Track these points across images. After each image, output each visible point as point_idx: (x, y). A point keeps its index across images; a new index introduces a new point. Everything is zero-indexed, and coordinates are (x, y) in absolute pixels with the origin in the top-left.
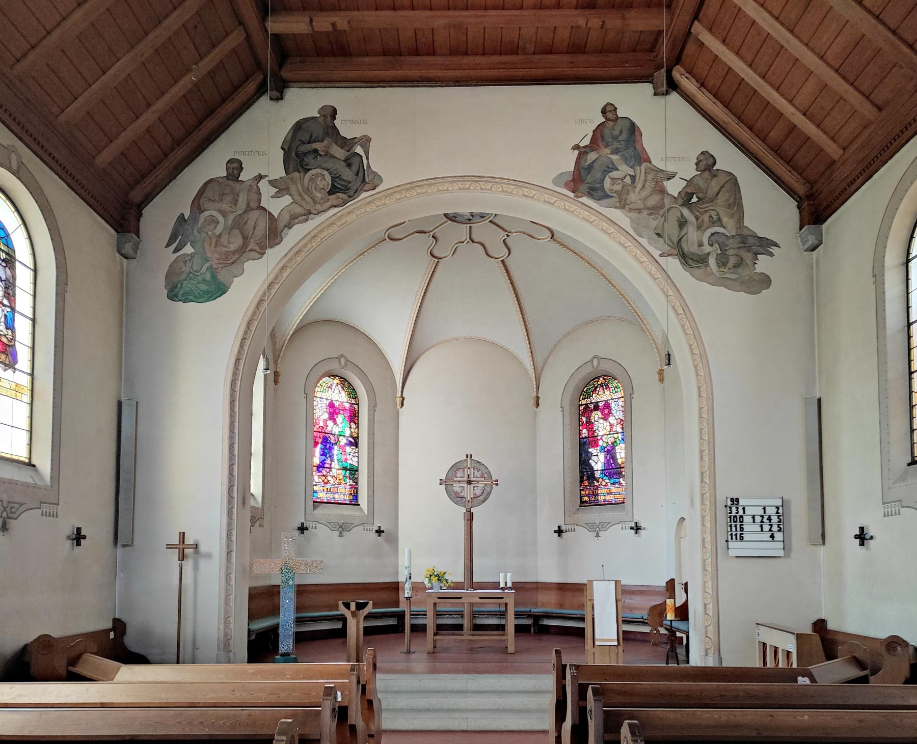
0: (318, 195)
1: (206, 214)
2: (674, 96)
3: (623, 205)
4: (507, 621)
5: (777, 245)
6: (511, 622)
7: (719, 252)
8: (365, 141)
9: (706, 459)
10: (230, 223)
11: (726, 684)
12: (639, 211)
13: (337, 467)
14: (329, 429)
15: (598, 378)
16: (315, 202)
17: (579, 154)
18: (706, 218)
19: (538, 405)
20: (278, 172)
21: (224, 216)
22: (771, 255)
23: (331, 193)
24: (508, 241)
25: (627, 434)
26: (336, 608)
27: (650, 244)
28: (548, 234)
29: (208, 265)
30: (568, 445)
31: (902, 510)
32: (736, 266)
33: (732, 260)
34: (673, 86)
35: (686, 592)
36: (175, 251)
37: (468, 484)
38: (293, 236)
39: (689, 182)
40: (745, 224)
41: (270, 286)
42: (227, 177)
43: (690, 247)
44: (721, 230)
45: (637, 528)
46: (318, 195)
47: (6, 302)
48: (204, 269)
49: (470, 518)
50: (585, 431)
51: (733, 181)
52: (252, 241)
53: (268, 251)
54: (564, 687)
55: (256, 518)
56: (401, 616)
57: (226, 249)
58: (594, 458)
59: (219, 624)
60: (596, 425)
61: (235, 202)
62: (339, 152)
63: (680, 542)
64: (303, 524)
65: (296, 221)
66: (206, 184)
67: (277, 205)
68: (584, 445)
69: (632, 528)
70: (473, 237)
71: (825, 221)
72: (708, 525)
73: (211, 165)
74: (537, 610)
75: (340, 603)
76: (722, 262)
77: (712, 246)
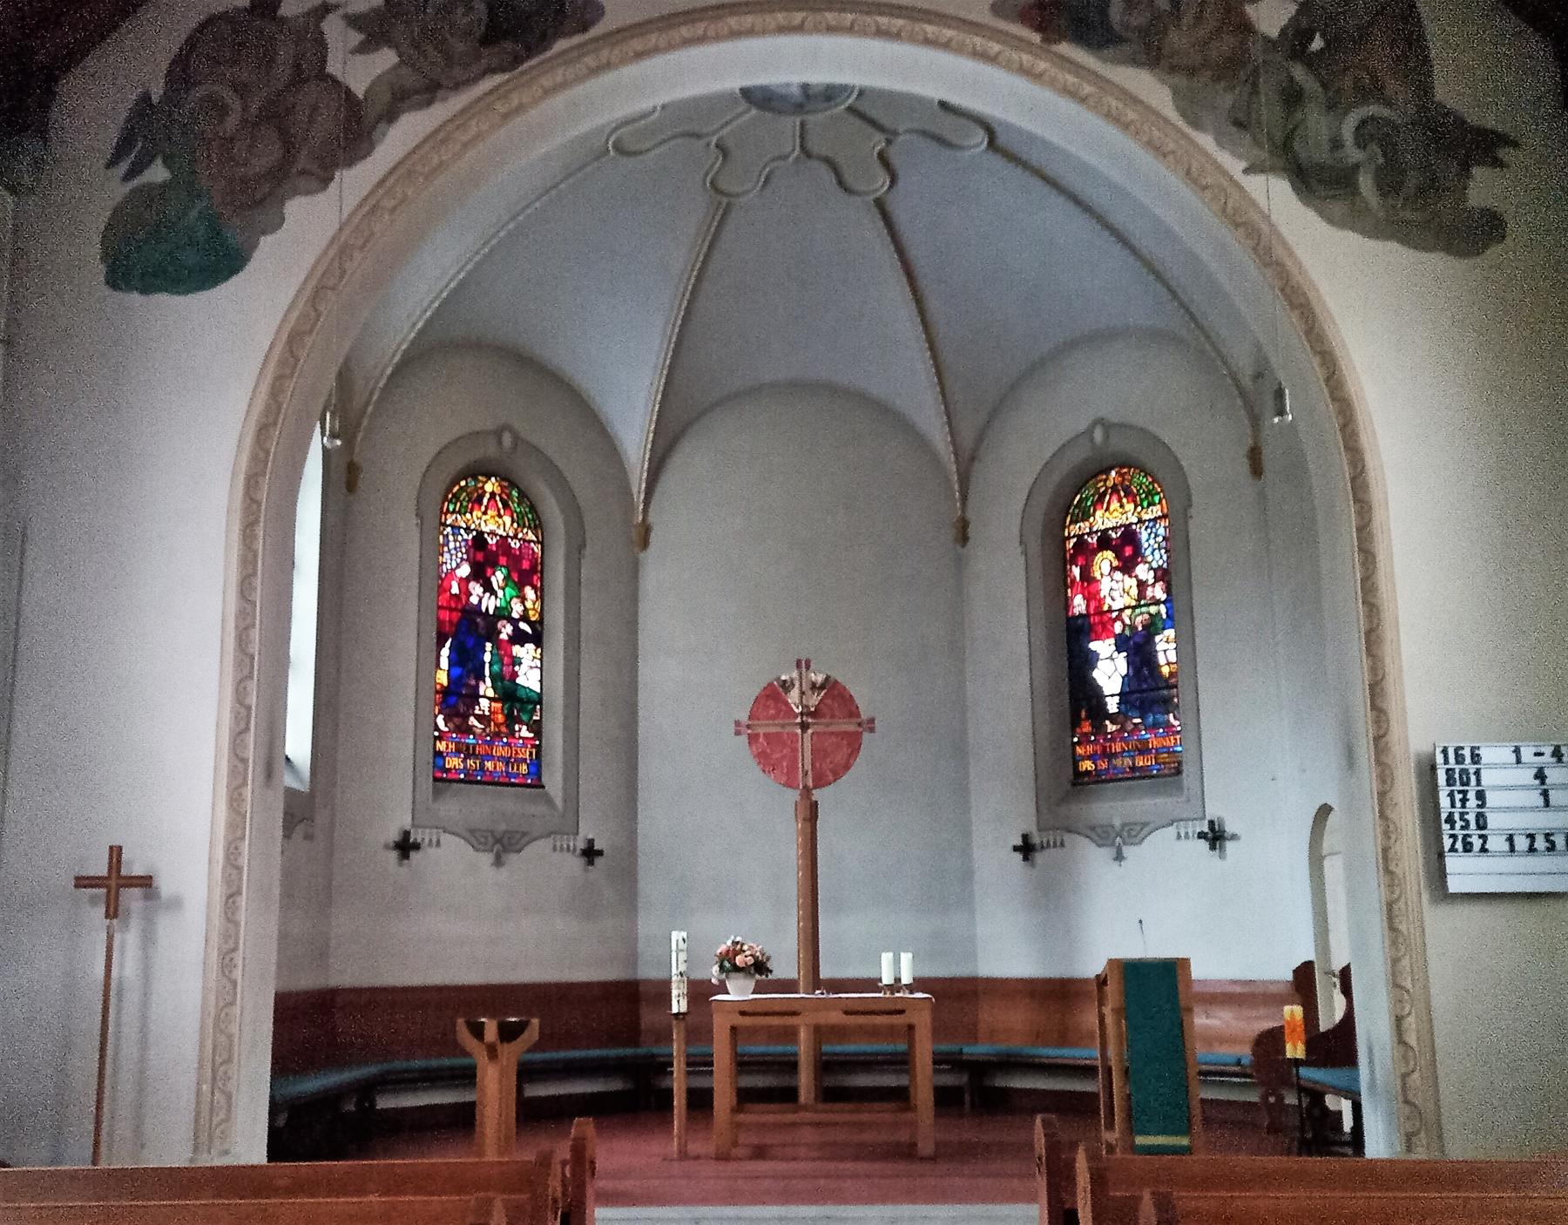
0: (460, 47)
1: (199, 92)
3: (1153, 55)
4: (913, 1078)
6: (924, 1081)
7: (1381, 160)
10: (254, 108)
12: (1192, 72)
13: (491, 693)
14: (474, 600)
15: (1107, 471)
16: (449, 59)
18: (1348, 82)
19: (963, 538)
22: (1498, 163)
23: (488, 40)
25: (1179, 603)
28: (980, 137)
30: (1040, 633)
32: (1421, 191)
33: (1412, 180)
35: (1347, 990)
36: (129, 176)
37: (810, 735)
38: (404, 134)
43: (1314, 148)
45: (1216, 837)
48: (194, 214)
49: (811, 814)
52: (304, 152)
55: (300, 814)
60: (1105, 586)
61: (269, 61)
63: (1321, 868)
67: (361, 70)
69: (1201, 835)
76: (1389, 184)
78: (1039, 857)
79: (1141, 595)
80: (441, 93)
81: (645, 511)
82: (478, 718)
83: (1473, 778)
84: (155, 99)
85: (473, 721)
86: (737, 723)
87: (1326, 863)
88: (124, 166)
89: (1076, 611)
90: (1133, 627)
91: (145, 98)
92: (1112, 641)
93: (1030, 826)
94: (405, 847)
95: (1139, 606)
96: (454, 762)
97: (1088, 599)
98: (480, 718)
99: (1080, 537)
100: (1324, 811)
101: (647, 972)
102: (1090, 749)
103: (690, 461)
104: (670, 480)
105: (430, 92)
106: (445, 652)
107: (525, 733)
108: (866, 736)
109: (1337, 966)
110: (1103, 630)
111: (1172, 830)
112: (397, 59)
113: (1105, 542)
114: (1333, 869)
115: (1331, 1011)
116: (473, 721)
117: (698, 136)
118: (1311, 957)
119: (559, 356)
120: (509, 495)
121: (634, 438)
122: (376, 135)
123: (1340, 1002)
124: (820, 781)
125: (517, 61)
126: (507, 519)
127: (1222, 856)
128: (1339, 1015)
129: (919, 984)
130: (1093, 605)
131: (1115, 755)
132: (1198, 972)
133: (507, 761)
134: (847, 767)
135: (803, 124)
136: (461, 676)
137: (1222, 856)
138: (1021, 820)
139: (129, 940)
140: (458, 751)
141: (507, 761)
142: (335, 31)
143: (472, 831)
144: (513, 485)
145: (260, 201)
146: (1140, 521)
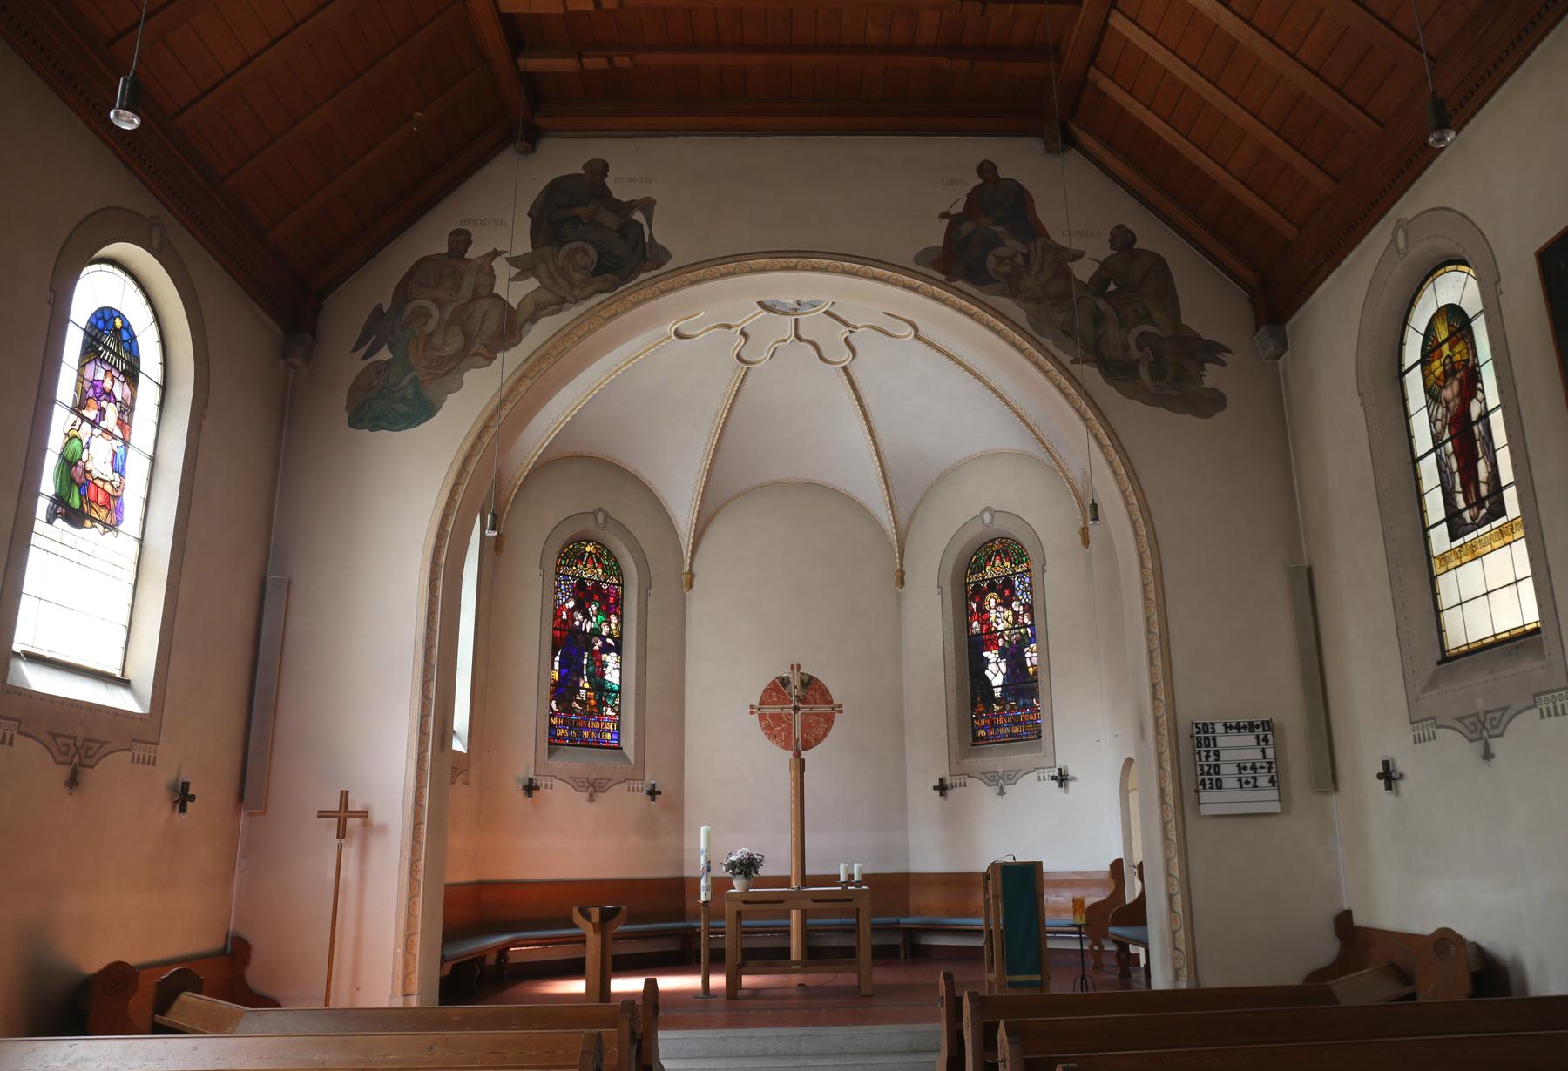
0: (577, 276)
1: (415, 304)
2: (1073, 156)
3: (1014, 292)
6: (866, 942)
8: (648, 206)
9: (1158, 662)
10: (447, 316)
11: (1206, 1013)
17: (950, 225)
19: (902, 583)
20: (523, 246)
22: (1223, 364)
23: (595, 273)
24: (852, 339)
29: (411, 376)
31: (1438, 731)
34: (1069, 141)
36: (365, 357)
37: (798, 709)
38: (538, 334)
39: (1104, 265)
41: (503, 402)
42: (448, 255)
45: (1062, 779)
46: (577, 276)
47: (118, 432)
50: (975, 624)
51: (1159, 263)
54: (960, 1034)
56: (691, 936)
57: (437, 354)
58: (992, 667)
59: (396, 947)
61: (458, 288)
62: (609, 219)
64: (531, 780)
66: (418, 263)
67: (515, 290)
68: (973, 649)
70: (801, 333)
71: (1289, 318)
74: (909, 920)
75: (576, 911)
77: (1141, 349)
78: (950, 793)
79: (1015, 621)
81: (691, 565)
85: (575, 704)
90: (1010, 642)
91: (379, 308)
93: (943, 771)
94: (530, 788)
96: (562, 732)
97: (981, 624)
98: (579, 702)
99: (976, 583)
100: (1129, 761)
101: (688, 873)
103: (719, 534)
105: (560, 304)
107: (609, 712)
109: (1137, 862)
110: (990, 645)
113: (992, 587)
114: (1134, 799)
115: (1131, 895)
116: (575, 704)
117: (729, 327)
118: (1121, 855)
119: (635, 464)
121: (684, 516)
123: (1138, 883)
124: (807, 746)
127: (1067, 792)
128: (1137, 893)
129: (866, 879)
132: (1045, 868)
134: (824, 736)
137: (1067, 792)
139: (351, 853)
140: (565, 724)
142: (501, 267)
144: (605, 547)
145: (449, 371)
146: (1014, 573)
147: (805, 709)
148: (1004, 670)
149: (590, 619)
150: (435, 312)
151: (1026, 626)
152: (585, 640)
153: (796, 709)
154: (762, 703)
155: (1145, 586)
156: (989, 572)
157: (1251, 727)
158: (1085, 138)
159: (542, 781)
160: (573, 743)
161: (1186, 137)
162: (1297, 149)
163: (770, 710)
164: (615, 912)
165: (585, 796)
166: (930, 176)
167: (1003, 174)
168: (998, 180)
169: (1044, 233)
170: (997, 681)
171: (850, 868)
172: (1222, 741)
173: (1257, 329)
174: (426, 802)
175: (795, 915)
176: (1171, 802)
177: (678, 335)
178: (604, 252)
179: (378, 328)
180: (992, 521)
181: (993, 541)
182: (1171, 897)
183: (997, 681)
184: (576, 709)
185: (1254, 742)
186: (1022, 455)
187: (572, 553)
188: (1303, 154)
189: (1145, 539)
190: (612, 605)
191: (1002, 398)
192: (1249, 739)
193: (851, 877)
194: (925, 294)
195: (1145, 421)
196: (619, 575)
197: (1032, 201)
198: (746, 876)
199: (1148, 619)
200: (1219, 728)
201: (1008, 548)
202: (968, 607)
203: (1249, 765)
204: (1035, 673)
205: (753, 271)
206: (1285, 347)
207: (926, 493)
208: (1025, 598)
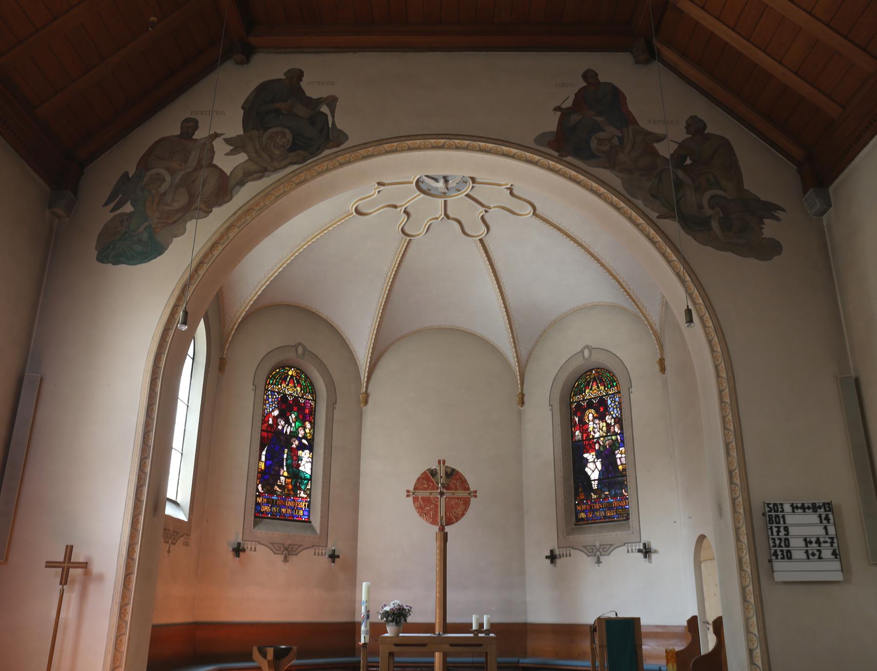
0: (277, 152)
1: (153, 171)
2: (656, 65)
3: (611, 164)
5: (783, 210)
7: (722, 215)
8: (332, 102)
9: (734, 453)
10: (177, 180)
13: (286, 474)
19: (522, 403)
20: (236, 129)
21: (171, 175)
22: (778, 219)
23: (291, 150)
24: (487, 217)
26: (249, 658)
27: (645, 205)
29: (146, 224)
36: (113, 210)
37: (443, 494)
39: (681, 145)
40: (745, 188)
42: (180, 136)
44: (722, 193)
45: (647, 551)
49: (445, 538)
50: (577, 433)
53: (215, 210)
58: (591, 465)
62: (302, 111)
64: (239, 544)
65: (250, 178)
67: (228, 162)
72: (744, 539)
73: (167, 125)
75: (255, 649)
77: (712, 208)
78: (558, 561)
79: (608, 430)
80: (266, 173)
81: (367, 387)
82: (279, 486)
83: (781, 520)
84: (130, 176)
85: (276, 488)
86: (408, 491)
87: (703, 565)
88: (112, 206)
89: (577, 439)
90: (604, 446)
91: (127, 173)
92: (594, 453)
93: (553, 545)
94: (238, 550)
95: (607, 436)
96: (266, 508)
97: (582, 432)
98: (280, 487)
99: (578, 402)
100: (702, 538)
101: (357, 619)
102: (584, 507)
103: (389, 365)
104: (378, 372)
105: (263, 172)
106: (264, 453)
107: (302, 495)
108: (472, 499)
109: (711, 617)
110: (589, 448)
111: (625, 548)
112: (247, 158)
113: (590, 405)
116: (276, 488)
117: (395, 207)
118: (696, 614)
119: (326, 312)
120: (300, 377)
121: (362, 352)
122: (234, 192)
124: (449, 522)
125: (304, 160)
126: (299, 389)
127: (650, 561)
129: (494, 627)
130: (585, 435)
131: (597, 510)
132: (643, 622)
133: (293, 509)
134: (463, 515)
135: (445, 201)
136: (271, 465)
137: (650, 561)
138: (551, 543)
139: (72, 598)
140: (268, 503)
141: (293, 509)
142: (219, 146)
143: (272, 544)
144: (303, 372)
145: (175, 221)
146: (607, 394)
147: (448, 494)
148: (600, 467)
149: (290, 424)
150: (168, 178)
151: (616, 434)
152: (287, 439)
153: (442, 494)
154: (415, 488)
155: (720, 392)
156: (588, 394)
157: (814, 508)
158: (667, 53)
159: (248, 545)
160: (274, 517)
161: (748, 40)
162: (845, 37)
163: (421, 494)
164: (287, 651)
165: (281, 557)
166: (549, 80)
167: (602, 79)
168: (599, 83)
169: (635, 122)
170: (594, 476)
171: (481, 619)
172: (791, 519)
173: (805, 193)
174: (137, 556)
175: (438, 658)
176: (749, 570)
177: (358, 212)
178: (299, 136)
179: (124, 189)
180: (590, 356)
181: (591, 371)
182: (751, 652)
183: (594, 476)
184: (276, 493)
185: (817, 520)
186: (613, 307)
187: (278, 373)
188: (850, 41)
189: (720, 354)
190: (307, 414)
191: (598, 261)
192: (813, 518)
193: (481, 625)
194: (542, 166)
195: (715, 262)
196: (313, 393)
197: (625, 98)
198: (397, 623)
199: (724, 418)
200: (787, 508)
201: (602, 375)
202: (572, 420)
203: (814, 540)
204: (624, 470)
205: (410, 149)
206: (829, 205)
207: (540, 337)
208: (615, 413)
